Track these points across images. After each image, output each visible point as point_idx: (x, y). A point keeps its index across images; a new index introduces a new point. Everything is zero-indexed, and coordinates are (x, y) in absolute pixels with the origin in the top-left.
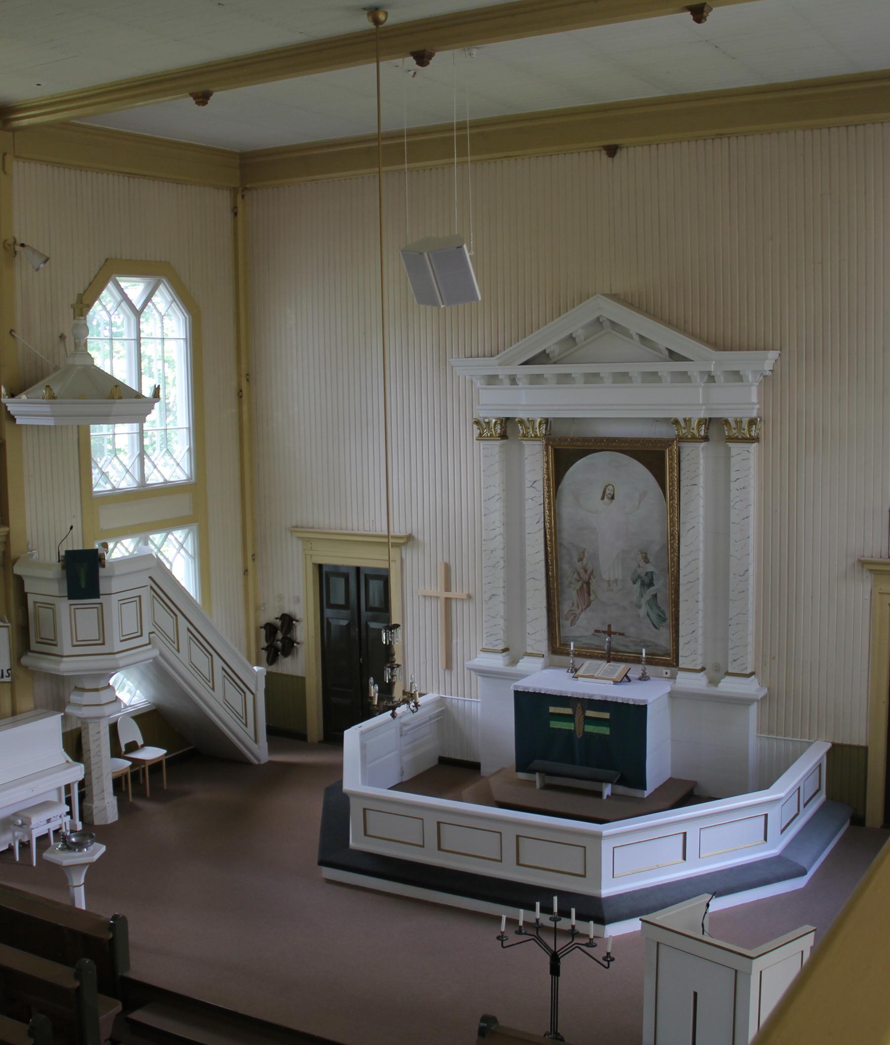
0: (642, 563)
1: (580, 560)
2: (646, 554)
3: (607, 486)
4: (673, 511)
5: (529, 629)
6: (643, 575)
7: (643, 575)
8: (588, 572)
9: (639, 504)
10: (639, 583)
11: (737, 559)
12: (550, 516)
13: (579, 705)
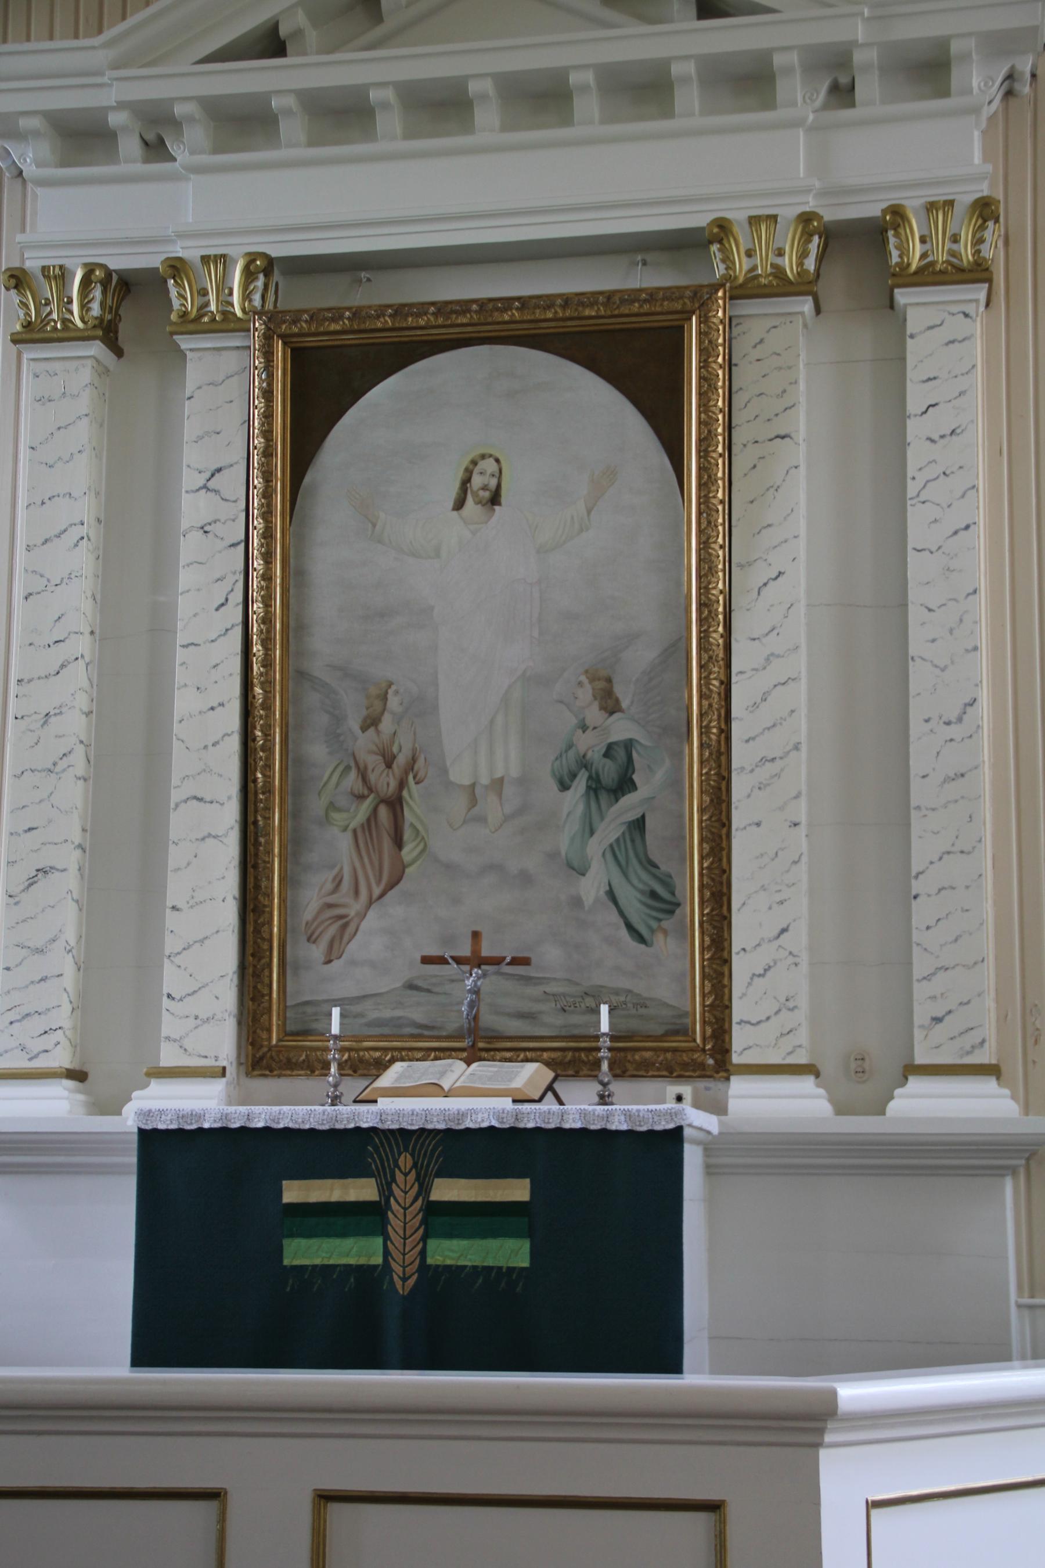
0: (594, 714)
1: (371, 722)
2: (609, 680)
3: (474, 463)
4: (709, 523)
5: (172, 979)
6: (595, 755)
7: (595, 755)
8: (395, 766)
9: (589, 512)
10: (580, 784)
11: (936, 666)
12: (267, 577)
13: (405, 1161)
